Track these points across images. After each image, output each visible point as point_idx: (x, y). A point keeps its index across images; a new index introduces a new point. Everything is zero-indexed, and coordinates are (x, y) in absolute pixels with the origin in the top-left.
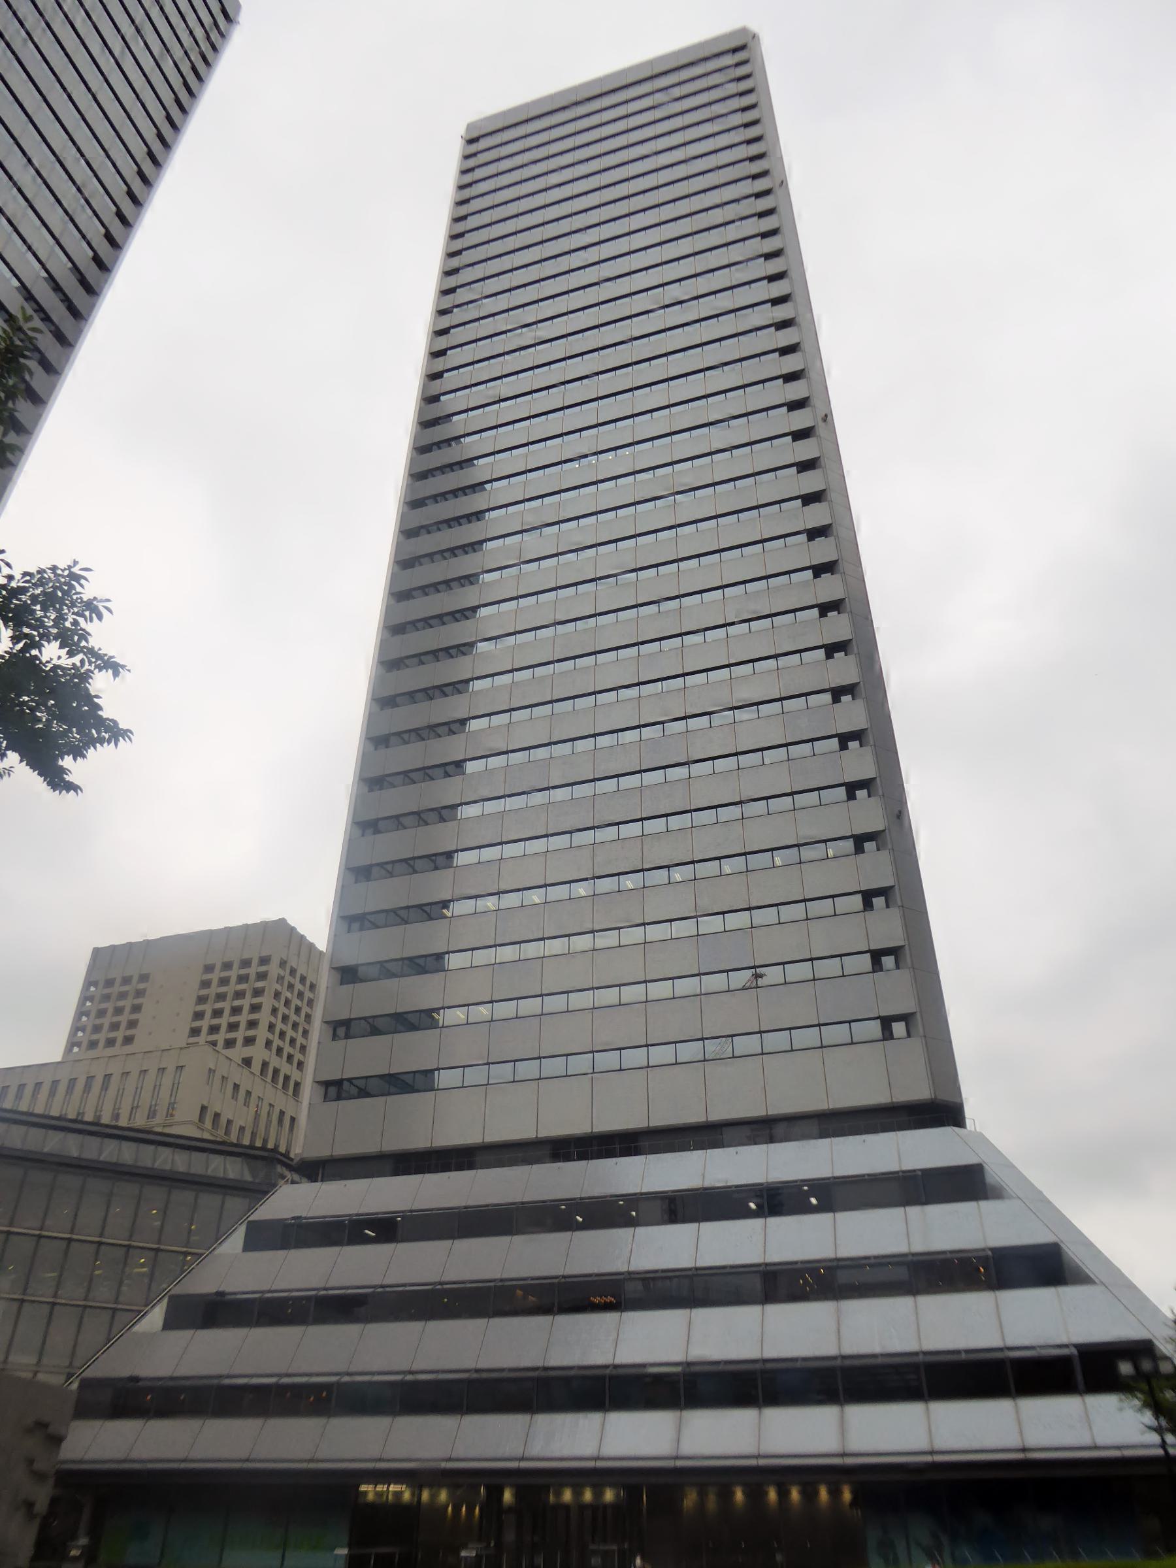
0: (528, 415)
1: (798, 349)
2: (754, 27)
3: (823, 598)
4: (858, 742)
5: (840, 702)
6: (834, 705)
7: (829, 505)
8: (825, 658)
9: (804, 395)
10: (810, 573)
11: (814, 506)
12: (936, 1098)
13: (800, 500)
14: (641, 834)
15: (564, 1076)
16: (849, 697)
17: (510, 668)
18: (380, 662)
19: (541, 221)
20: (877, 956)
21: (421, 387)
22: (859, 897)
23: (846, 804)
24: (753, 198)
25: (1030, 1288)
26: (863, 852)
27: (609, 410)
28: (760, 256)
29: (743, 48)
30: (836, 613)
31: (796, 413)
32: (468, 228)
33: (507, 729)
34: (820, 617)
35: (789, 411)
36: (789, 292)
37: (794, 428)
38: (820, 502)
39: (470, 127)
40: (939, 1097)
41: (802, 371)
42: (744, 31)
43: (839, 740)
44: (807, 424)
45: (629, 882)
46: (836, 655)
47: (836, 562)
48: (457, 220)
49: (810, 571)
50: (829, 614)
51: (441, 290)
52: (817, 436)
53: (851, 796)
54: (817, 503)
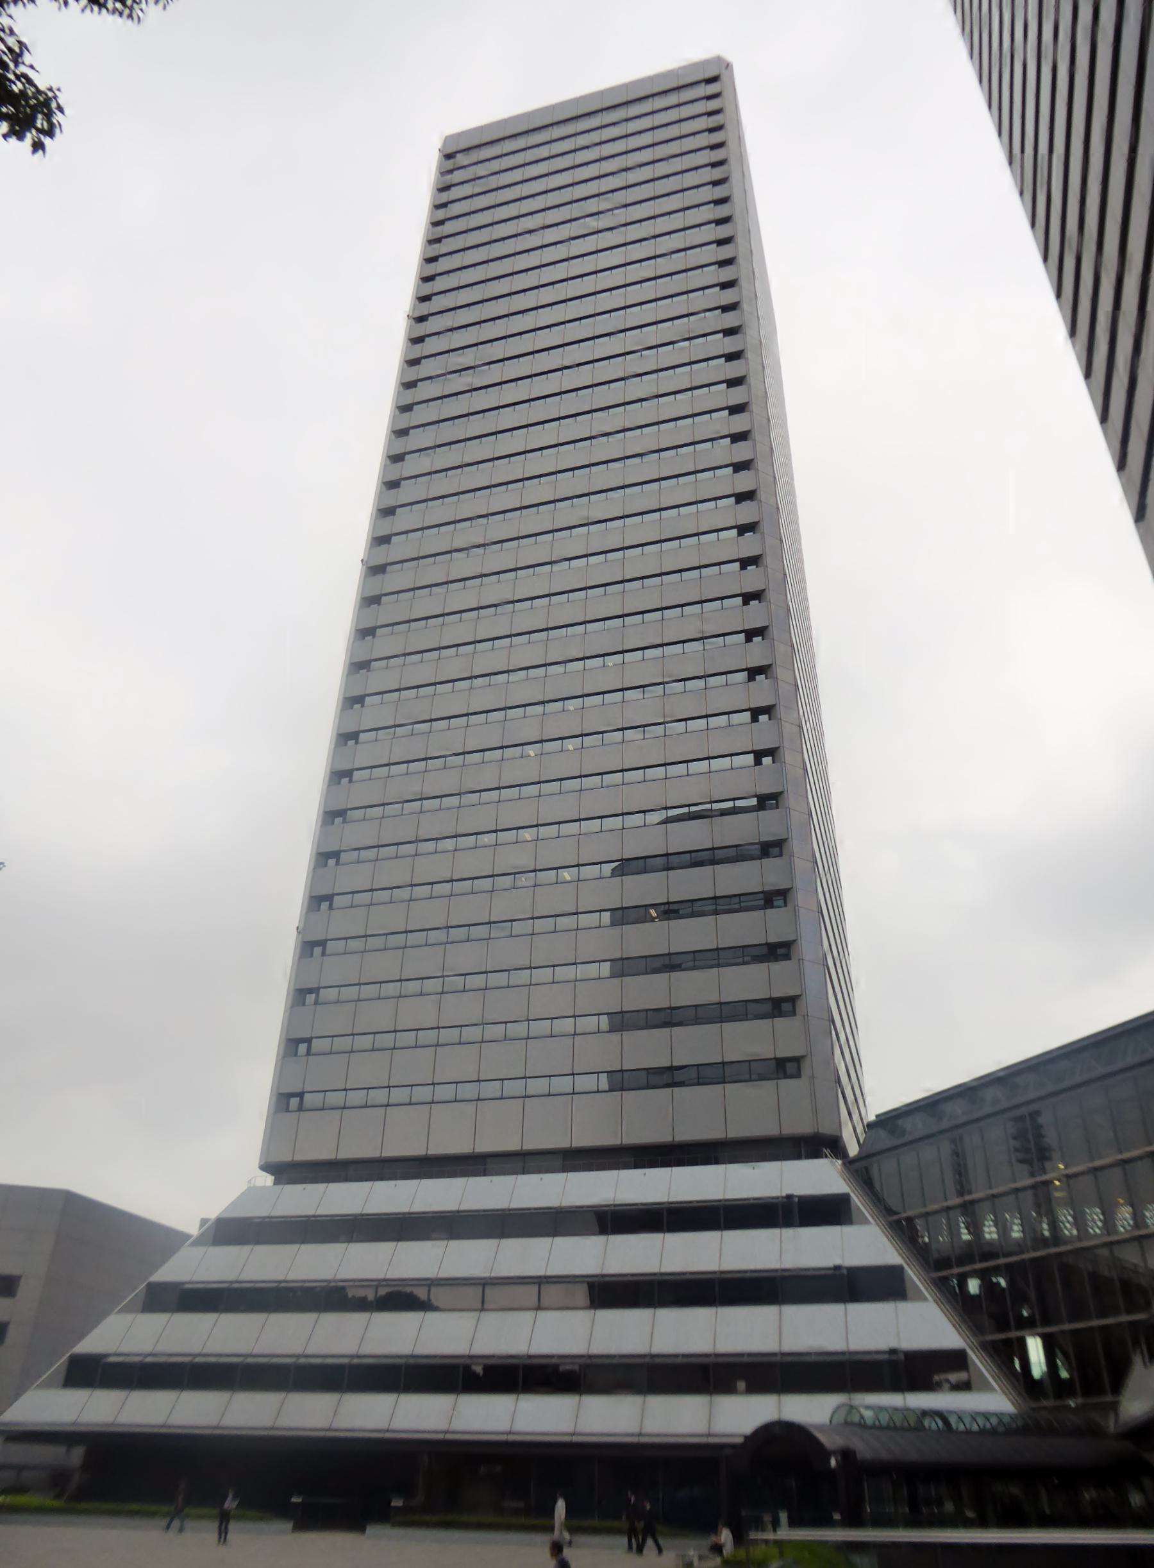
0: (491, 457)
1: (746, 410)
2: (730, 58)
3: (742, 521)
4: (771, 758)
5: (752, 641)
6: (753, 724)
7: (778, 723)
8: (744, 641)
9: (735, 300)
10: (734, 532)
11: (743, 474)
12: (818, 1132)
13: (738, 563)
14: (581, 747)
15: (506, 1079)
16: (766, 717)
17: (476, 606)
18: (298, 990)
19: (522, 162)
20: (759, 755)
21: (416, 287)
22: (748, 713)
23: (750, 725)
24: (713, 225)
25: (890, 1393)
26: (757, 721)
27: (570, 430)
28: (709, 203)
29: (714, 80)
30: (755, 567)
31: (737, 417)
32: (439, 271)
33: (469, 723)
34: (744, 605)
35: (730, 414)
36: (756, 520)
37: (731, 403)
38: (746, 440)
39: (448, 140)
40: (820, 1131)
41: (740, 327)
42: (719, 60)
43: (746, 637)
44: (735, 324)
45: (566, 875)
46: (757, 677)
47: (760, 556)
48: (436, 224)
49: (738, 564)
50: (749, 568)
51: (425, 258)
52: (758, 500)
53: (755, 719)
54: (749, 502)
